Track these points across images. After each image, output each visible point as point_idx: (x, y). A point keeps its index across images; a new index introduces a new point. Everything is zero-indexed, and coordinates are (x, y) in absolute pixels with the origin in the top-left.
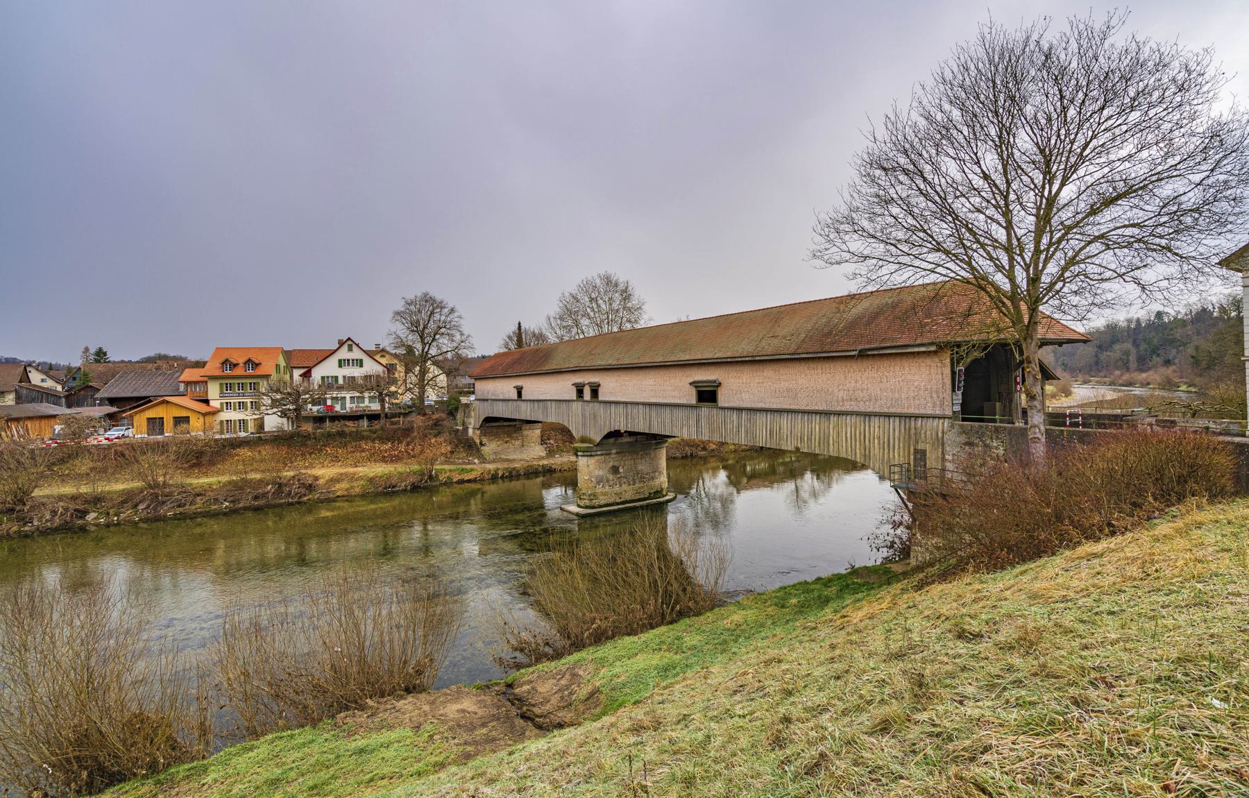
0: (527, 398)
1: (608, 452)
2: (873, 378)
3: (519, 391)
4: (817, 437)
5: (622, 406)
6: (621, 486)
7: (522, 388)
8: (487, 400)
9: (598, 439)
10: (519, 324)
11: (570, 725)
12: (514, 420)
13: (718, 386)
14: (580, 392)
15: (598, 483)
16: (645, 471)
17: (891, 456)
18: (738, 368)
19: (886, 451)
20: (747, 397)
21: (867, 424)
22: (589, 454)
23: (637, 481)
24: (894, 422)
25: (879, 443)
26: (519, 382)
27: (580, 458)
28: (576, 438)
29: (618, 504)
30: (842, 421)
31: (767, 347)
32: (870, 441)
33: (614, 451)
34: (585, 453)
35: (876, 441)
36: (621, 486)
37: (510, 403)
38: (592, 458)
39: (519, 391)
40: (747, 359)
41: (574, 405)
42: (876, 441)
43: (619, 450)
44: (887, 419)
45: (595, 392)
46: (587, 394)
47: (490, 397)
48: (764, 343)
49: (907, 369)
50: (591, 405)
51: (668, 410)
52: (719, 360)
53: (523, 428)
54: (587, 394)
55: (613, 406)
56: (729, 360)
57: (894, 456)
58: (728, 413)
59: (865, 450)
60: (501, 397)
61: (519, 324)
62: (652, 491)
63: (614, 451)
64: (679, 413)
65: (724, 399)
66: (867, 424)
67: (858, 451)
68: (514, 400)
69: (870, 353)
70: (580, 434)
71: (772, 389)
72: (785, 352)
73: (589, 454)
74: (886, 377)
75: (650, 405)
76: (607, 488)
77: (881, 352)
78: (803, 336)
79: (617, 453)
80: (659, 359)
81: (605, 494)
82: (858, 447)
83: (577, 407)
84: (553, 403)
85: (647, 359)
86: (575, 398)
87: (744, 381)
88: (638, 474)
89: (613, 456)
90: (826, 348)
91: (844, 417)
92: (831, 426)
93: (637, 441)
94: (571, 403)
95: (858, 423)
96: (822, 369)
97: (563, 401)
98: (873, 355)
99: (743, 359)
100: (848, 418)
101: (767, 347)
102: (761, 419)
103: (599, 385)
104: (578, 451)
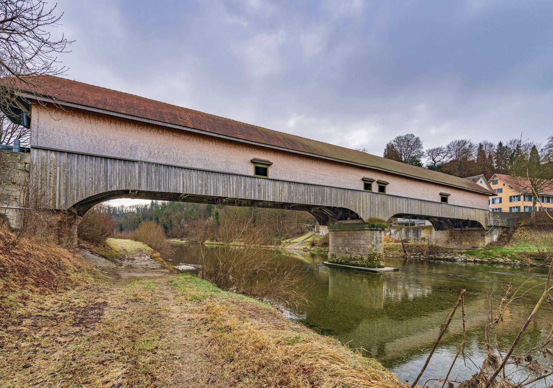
3: (444, 199)
8: (133, 161)
14: (368, 187)
39: (444, 199)
44: (168, 167)
46: (375, 188)
54: (375, 188)
65: (272, 173)
83: (366, 196)
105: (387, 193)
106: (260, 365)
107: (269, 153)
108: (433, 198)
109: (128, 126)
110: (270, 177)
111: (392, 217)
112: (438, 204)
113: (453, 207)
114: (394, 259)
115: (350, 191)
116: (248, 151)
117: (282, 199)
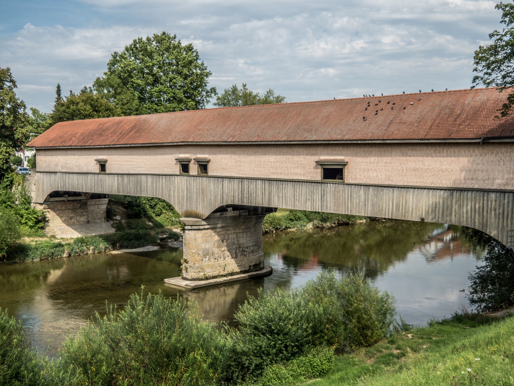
0: (214, 174)
1: (214, 226)
2: (492, 161)
3: (103, 166)
4: (441, 210)
5: (236, 181)
6: (224, 259)
7: (106, 161)
8: (55, 173)
9: (206, 213)
10: (59, 87)
11: (444, 323)
12: (78, 194)
13: (345, 165)
14: (185, 167)
15: (205, 256)
16: (246, 245)
17: (505, 224)
18: (366, 149)
19: (501, 220)
20: (375, 174)
21: (485, 198)
22: (196, 227)
23: (239, 254)
24: (509, 197)
25: (495, 214)
26: (102, 157)
27: (187, 232)
28: (180, 213)
29: (222, 276)
30: (463, 196)
31: (396, 132)
32: (487, 212)
33: (219, 225)
34: (194, 227)
35: (493, 212)
36: (224, 259)
37: (90, 176)
38: (199, 232)
39: (103, 166)
40: (378, 142)
41: (177, 179)
42: (493, 212)
43: (224, 225)
44: (502, 194)
45: (204, 166)
46: (194, 169)
47: (59, 169)
48: (392, 128)
49: (471, 152)
50: (199, 180)
51: (290, 185)
52: (349, 142)
53: (89, 203)
54: (194, 169)
55: (226, 181)
56: (359, 142)
57: (507, 224)
58: (355, 189)
59: (483, 218)
60: (77, 171)
61: (59, 87)
62: (252, 264)
63: (219, 225)
64: (304, 189)
65: (349, 176)
66: (485, 198)
67: (477, 220)
68: (95, 174)
69: (492, 141)
70: (185, 209)
71: (400, 168)
72: (416, 137)
73: (196, 227)
74: (504, 161)
75: (270, 180)
76: (213, 260)
77: (502, 141)
78: (429, 123)
79: (222, 227)
80: (283, 137)
81: (212, 267)
82: (477, 217)
83: (182, 182)
84: (149, 177)
85: (269, 136)
86: (98, 171)
87: (372, 161)
88: (240, 247)
89: (218, 230)
90: (453, 136)
91: (466, 193)
92: (454, 200)
93: (240, 215)
94: (173, 178)
95: (478, 198)
96: (447, 152)
97: (162, 175)
98: (493, 143)
99: (374, 142)
100: (470, 193)
101: (396, 132)
102: (387, 194)
103: (209, 161)
104: (185, 225)
105: (210, 173)
106: (16, 330)
107: (445, 151)
108: (242, 174)
109: (337, 148)
110: (346, 182)
111: (212, 213)
112: (310, 186)
113: (362, 190)
114: (59, 259)
115: (164, 177)
116: (181, 149)
117: (316, 209)
